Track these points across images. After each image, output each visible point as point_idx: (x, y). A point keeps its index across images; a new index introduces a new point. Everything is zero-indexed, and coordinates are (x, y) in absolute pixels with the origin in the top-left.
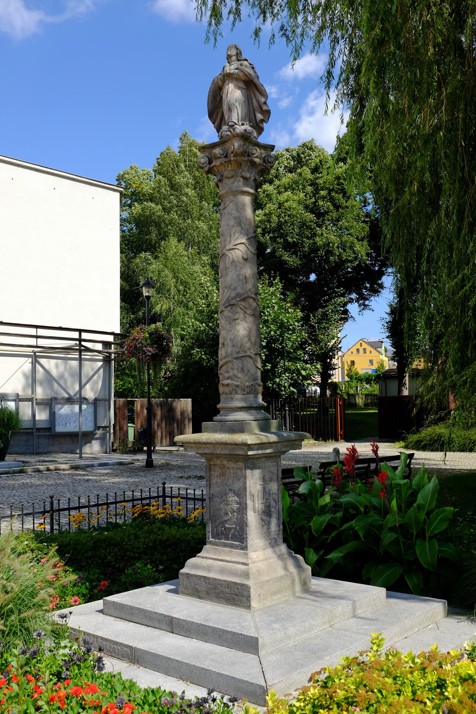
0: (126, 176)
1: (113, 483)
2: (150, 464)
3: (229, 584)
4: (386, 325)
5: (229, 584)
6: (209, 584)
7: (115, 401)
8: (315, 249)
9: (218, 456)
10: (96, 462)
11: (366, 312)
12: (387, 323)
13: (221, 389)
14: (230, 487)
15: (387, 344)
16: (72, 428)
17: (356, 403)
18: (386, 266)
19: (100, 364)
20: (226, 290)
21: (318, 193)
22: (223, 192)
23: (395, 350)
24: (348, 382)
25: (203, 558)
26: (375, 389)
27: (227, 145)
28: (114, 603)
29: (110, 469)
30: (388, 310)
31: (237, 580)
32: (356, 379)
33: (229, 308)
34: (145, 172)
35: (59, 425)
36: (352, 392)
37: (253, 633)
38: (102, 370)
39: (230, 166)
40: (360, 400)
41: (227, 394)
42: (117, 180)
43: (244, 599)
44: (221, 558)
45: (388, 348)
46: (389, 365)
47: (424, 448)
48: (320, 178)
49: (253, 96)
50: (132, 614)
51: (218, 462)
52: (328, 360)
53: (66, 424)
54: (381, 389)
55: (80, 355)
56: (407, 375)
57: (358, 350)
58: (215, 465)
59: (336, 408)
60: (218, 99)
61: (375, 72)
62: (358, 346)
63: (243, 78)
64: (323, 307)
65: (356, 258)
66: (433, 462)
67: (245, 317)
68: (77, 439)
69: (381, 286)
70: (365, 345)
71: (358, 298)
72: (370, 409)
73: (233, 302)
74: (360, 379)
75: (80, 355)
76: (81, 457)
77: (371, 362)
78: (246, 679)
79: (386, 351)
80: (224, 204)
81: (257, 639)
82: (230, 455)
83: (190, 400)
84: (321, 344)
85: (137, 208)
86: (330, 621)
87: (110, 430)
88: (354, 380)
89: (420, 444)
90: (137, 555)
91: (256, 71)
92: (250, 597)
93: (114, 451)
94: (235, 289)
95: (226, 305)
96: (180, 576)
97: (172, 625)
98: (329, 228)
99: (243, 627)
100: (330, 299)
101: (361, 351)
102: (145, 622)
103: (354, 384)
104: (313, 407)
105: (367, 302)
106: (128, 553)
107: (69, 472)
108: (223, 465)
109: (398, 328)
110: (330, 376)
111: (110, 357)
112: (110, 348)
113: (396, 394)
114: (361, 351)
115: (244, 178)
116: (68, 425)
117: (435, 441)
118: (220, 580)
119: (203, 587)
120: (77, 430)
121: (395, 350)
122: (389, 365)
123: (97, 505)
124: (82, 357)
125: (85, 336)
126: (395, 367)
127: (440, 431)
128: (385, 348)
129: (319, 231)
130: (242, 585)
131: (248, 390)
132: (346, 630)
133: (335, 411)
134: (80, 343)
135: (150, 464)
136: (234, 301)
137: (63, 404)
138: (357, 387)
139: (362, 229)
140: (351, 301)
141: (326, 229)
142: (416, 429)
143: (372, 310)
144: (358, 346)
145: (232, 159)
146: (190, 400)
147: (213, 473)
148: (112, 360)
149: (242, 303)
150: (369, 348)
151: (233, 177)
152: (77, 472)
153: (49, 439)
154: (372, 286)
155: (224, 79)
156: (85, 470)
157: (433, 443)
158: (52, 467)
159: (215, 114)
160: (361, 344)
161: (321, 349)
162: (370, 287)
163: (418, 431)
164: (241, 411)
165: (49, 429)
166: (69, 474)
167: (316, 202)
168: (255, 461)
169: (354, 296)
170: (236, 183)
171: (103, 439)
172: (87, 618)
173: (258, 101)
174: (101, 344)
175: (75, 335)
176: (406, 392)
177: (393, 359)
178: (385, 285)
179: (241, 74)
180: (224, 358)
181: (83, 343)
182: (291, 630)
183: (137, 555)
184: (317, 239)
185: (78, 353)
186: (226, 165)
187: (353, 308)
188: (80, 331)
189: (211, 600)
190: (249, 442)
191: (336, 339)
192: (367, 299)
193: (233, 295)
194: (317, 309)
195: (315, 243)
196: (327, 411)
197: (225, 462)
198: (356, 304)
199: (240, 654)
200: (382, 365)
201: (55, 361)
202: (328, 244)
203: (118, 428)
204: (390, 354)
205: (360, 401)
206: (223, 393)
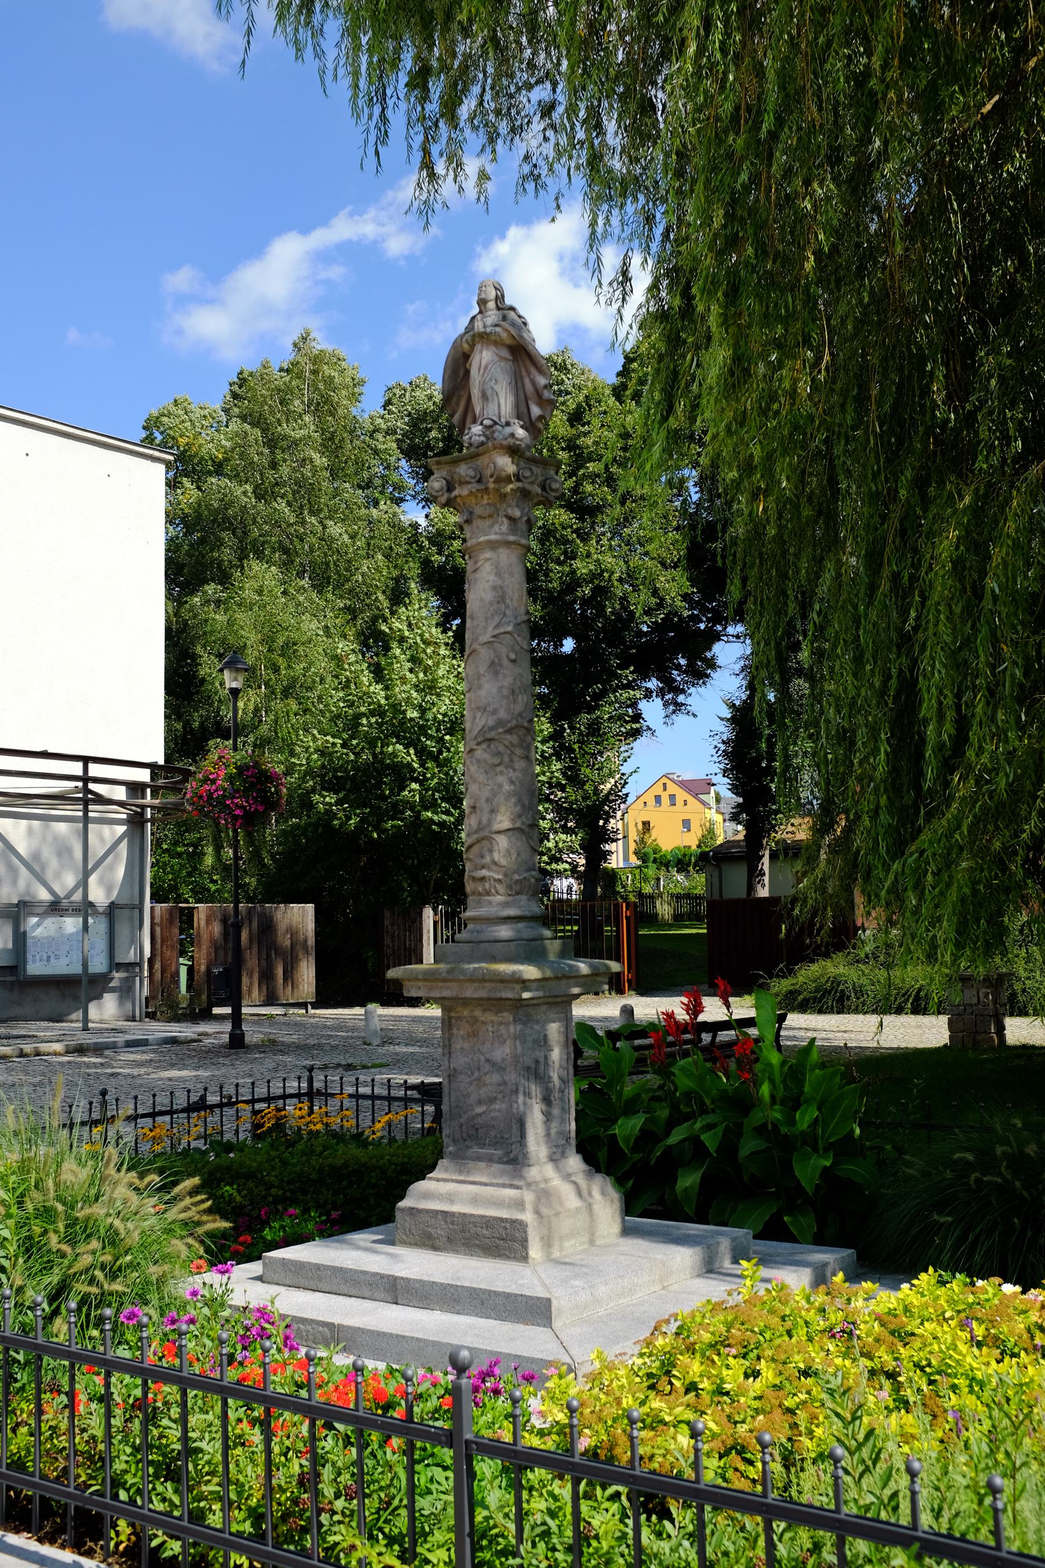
0: (165, 419)
1: (170, 1079)
2: (237, 1041)
4: (723, 747)
5: (489, 1222)
6: (453, 1223)
7: (152, 908)
8: (573, 583)
9: (466, 1002)
10: (121, 1039)
11: (680, 719)
12: (724, 742)
13: (469, 888)
14: (488, 1056)
15: (723, 786)
16: (65, 965)
17: (657, 915)
18: (725, 621)
19: (121, 829)
20: (479, 715)
21: (582, 466)
23: (740, 800)
24: (639, 867)
25: (438, 1180)
26: (697, 883)
27: (483, 461)
28: (284, 1262)
29: (154, 1051)
30: (727, 714)
31: (504, 1214)
32: (655, 861)
33: (484, 746)
34: (206, 412)
35: (34, 961)
36: (647, 889)
37: (540, 1292)
38: (124, 844)
40: (666, 907)
41: (480, 894)
42: (144, 428)
43: (517, 1246)
44: (471, 1179)
45: (722, 794)
46: (728, 831)
47: (803, 1008)
48: (585, 434)
49: (524, 373)
50: (320, 1279)
51: (466, 1013)
52: (601, 823)
53: (49, 958)
54: (709, 883)
55: (86, 811)
56: (767, 853)
57: (658, 799)
58: (459, 1018)
59: (618, 924)
60: (461, 373)
61: (720, 294)
62: (658, 790)
63: (508, 341)
64: (591, 710)
65: (660, 606)
66: (823, 1035)
67: (511, 761)
68: (74, 990)
69: (712, 664)
70: (672, 788)
71: (661, 689)
72: (687, 927)
73: (492, 734)
74: (663, 863)
75: (86, 811)
76: (85, 1029)
77: (686, 824)
78: (540, 1356)
79: (718, 800)
80: (476, 563)
81: (549, 1300)
82: (489, 999)
83: (310, 907)
84: (586, 787)
85: (190, 493)
86: (662, 1280)
87: (141, 970)
88: (650, 864)
89: (795, 999)
90: (288, 1194)
91: (522, 313)
92: (526, 1240)
93: (151, 1016)
95: (480, 739)
96: (398, 1214)
97: (395, 1290)
98: (605, 541)
99: (523, 1285)
100: (603, 694)
101: (665, 800)
102: (344, 1289)
103: (651, 871)
104: (569, 922)
105: (681, 698)
106: (273, 1191)
107: (66, 1059)
108: (475, 1018)
109: (751, 757)
110: (605, 855)
111: (142, 814)
112: (143, 797)
113: (742, 894)
114: (665, 800)
115: (510, 518)
116: (52, 960)
117: (827, 992)
118: (472, 1215)
119: (440, 1231)
120: (77, 969)
121: (740, 800)
122: (728, 831)
123: (153, 1115)
124: (91, 814)
125: (95, 770)
126: (741, 837)
127: (837, 971)
128: (717, 795)
129: (582, 549)
130: (513, 1222)
131: (518, 888)
132: (689, 1293)
133: (618, 931)
134: (85, 785)
135: (237, 1041)
137: (43, 915)
138: (658, 879)
139: (670, 543)
140: (648, 694)
141: (598, 542)
142: (787, 966)
143: (695, 715)
144: (658, 790)
145: (491, 486)
146: (310, 907)
147: (455, 1031)
148: (148, 821)
149: (508, 736)
150: (681, 795)
151: (490, 516)
152: (85, 1059)
153: (12, 990)
154: (691, 664)
155: (473, 340)
156: (101, 1055)
157: (823, 996)
158: (28, 1048)
159: (455, 399)
160: (665, 785)
161: (585, 798)
162: (687, 665)
163: (790, 972)
164: (505, 923)
165: (12, 969)
166: (69, 1062)
167: (578, 484)
168: (530, 1010)
169: (653, 684)
171: (125, 991)
172: (244, 1286)
173: (533, 383)
174: (123, 788)
175: (76, 768)
176: (763, 892)
177: (735, 818)
178: (719, 662)
179: (504, 335)
180: (476, 832)
181: (92, 786)
182: (602, 1290)
183: (288, 1194)
184: (577, 564)
185: (81, 807)
187: (652, 710)
188: (86, 760)
189: (457, 1252)
190: (526, 976)
191: (618, 776)
192: (683, 691)
193: (491, 722)
194: (577, 713)
195: (573, 572)
196: (602, 931)
197: (478, 1013)
198: (658, 702)
199: (520, 1327)
200: (711, 832)
201: (24, 823)
202: (601, 574)
203: (158, 966)
204: (728, 810)
205: (664, 910)
206: (473, 893)
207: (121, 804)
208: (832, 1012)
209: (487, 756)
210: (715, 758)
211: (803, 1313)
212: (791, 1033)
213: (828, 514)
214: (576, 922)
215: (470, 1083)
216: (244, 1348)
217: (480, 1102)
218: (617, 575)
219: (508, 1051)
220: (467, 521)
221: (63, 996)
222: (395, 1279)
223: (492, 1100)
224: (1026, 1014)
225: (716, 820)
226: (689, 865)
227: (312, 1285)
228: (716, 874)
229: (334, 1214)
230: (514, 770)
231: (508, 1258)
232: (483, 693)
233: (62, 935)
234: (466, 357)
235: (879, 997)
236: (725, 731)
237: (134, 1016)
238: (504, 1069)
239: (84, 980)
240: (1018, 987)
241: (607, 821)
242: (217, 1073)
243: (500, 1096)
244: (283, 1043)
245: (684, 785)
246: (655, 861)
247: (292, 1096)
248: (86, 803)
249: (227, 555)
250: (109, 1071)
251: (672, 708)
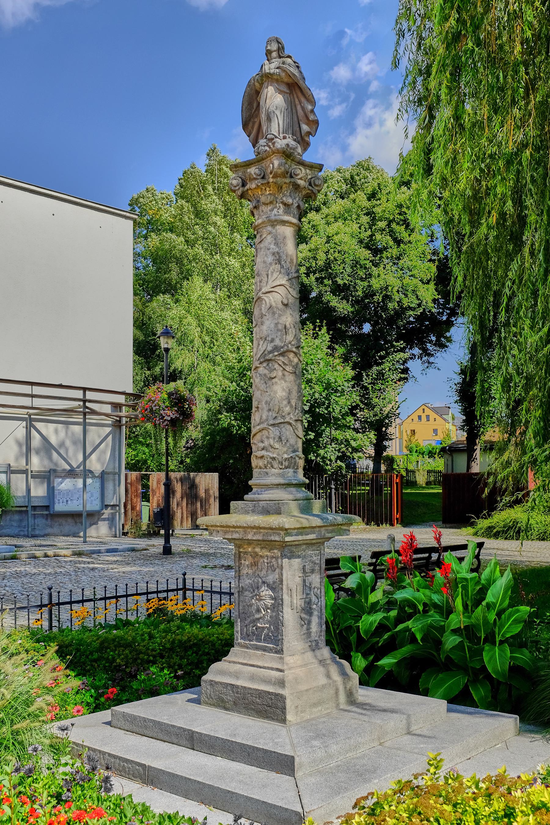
0: (141, 200)
3: (261, 693)
4: (455, 387)
5: (261, 694)
6: (237, 693)
8: (370, 294)
9: (250, 542)
10: (103, 548)
11: (431, 371)
14: (264, 579)
16: (74, 506)
17: (416, 481)
19: (108, 430)
20: (261, 343)
25: (230, 662)
32: (416, 451)
33: (265, 364)
34: (164, 196)
35: (59, 503)
36: (411, 467)
37: (288, 751)
39: (268, 189)
42: (130, 205)
46: (459, 436)
49: (297, 102)
51: (250, 549)
52: (384, 429)
53: (67, 501)
54: (446, 465)
55: (85, 419)
57: (420, 417)
60: (255, 105)
62: (420, 412)
64: (378, 364)
65: (419, 305)
68: (79, 519)
69: (449, 340)
70: (428, 412)
72: (432, 488)
75: (85, 419)
76: (85, 542)
77: (435, 431)
81: (293, 757)
86: (379, 739)
88: (414, 453)
90: (151, 658)
92: (285, 709)
94: (272, 341)
97: (194, 741)
99: (277, 744)
101: (424, 418)
105: (432, 359)
106: (141, 656)
110: (385, 448)
113: (464, 471)
114: (424, 418)
115: (285, 204)
116: (69, 502)
117: (510, 528)
119: (229, 697)
120: (80, 508)
124: (87, 421)
125: (90, 395)
128: (453, 415)
130: (277, 695)
131: (287, 464)
133: (391, 490)
136: (271, 355)
137: (64, 478)
140: (413, 357)
141: (384, 268)
142: (488, 513)
144: (420, 412)
145: (271, 180)
149: (281, 358)
150: (433, 415)
151: (271, 203)
152: (80, 559)
153: (47, 519)
154: (438, 340)
157: (508, 530)
158: (50, 553)
159: (251, 124)
160: (424, 409)
162: (436, 341)
165: (47, 507)
169: (416, 351)
170: (276, 210)
173: (303, 108)
175: (79, 394)
177: (462, 428)
178: (454, 339)
181: (88, 404)
182: (334, 748)
183: (151, 658)
185: (82, 417)
188: (85, 389)
189: (240, 712)
193: (269, 348)
194: (370, 367)
197: (257, 550)
199: (273, 775)
205: (421, 479)
207: (107, 415)
208: (513, 539)
210: (450, 394)
211: (472, 803)
212: (488, 551)
213: (517, 240)
214: (368, 485)
216: (69, 790)
218: (396, 289)
220: (255, 207)
221: (76, 523)
222: (193, 732)
225: (453, 431)
226: (435, 454)
227: (141, 731)
228: (450, 459)
229: (180, 673)
230: (285, 381)
231: (273, 719)
232: (264, 328)
233: (75, 489)
234: (258, 93)
235: (540, 531)
236: (458, 379)
237: (116, 534)
239: (84, 514)
241: (387, 428)
242: (152, 569)
244: (194, 552)
245: (434, 410)
246: (416, 451)
247: (172, 590)
248: (85, 414)
249: (174, 275)
250: (91, 566)
251: (426, 365)
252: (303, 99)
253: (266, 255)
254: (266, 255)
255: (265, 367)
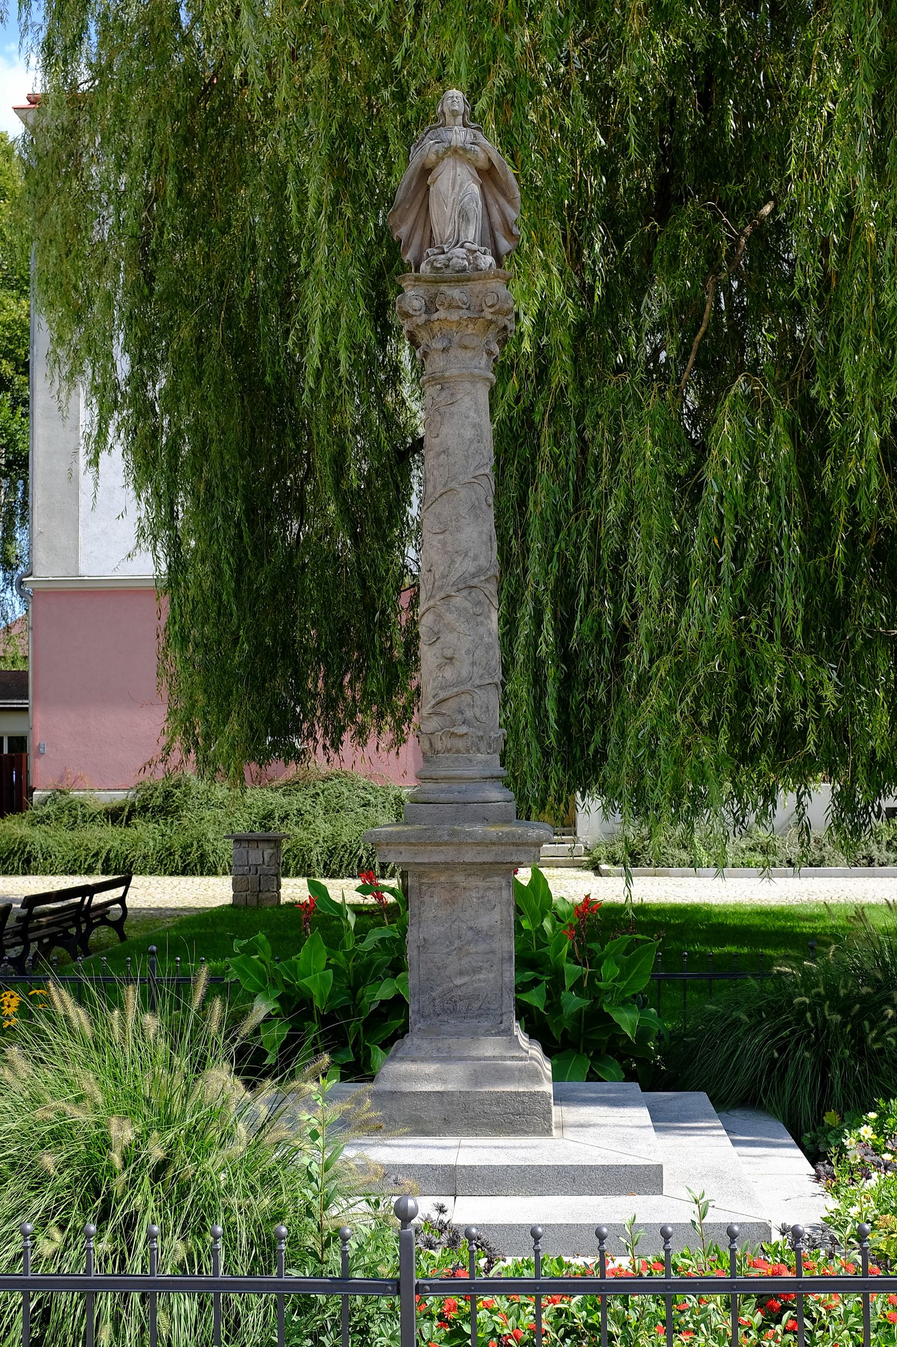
3: (501, 1097)
22: (455, 372)
33: (465, 593)
39: (471, 326)
51: (442, 879)
58: (430, 885)
94: (475, 558)
117: (12, 853)
130: (533, 1094)
136: (476, 580)
147: (427, 899)
170: (477, 359)
179: (482, 156)
186: (465, 323)
193: (472, 570)
208: (17, 873)
209: (468, 605)
215: (449, 954)
217: (461, 973)
219: (498, 917)
222: (454, 1168)
223: (477, 970)
224: (215, 874)
235: (67, 858)
238: (492, 937)
240: (208, 848)
243: (486, 965)
252: (502, 200)
253: (463, 425)
254: (463, 425)
255: (466, 598)
